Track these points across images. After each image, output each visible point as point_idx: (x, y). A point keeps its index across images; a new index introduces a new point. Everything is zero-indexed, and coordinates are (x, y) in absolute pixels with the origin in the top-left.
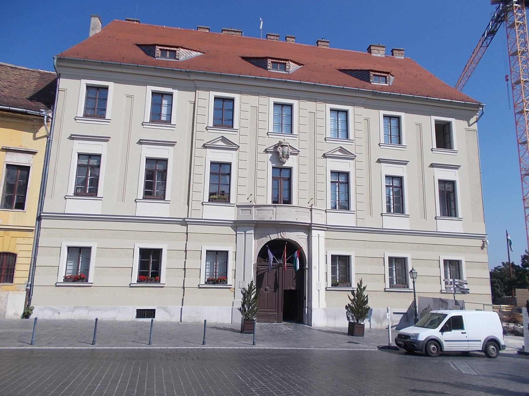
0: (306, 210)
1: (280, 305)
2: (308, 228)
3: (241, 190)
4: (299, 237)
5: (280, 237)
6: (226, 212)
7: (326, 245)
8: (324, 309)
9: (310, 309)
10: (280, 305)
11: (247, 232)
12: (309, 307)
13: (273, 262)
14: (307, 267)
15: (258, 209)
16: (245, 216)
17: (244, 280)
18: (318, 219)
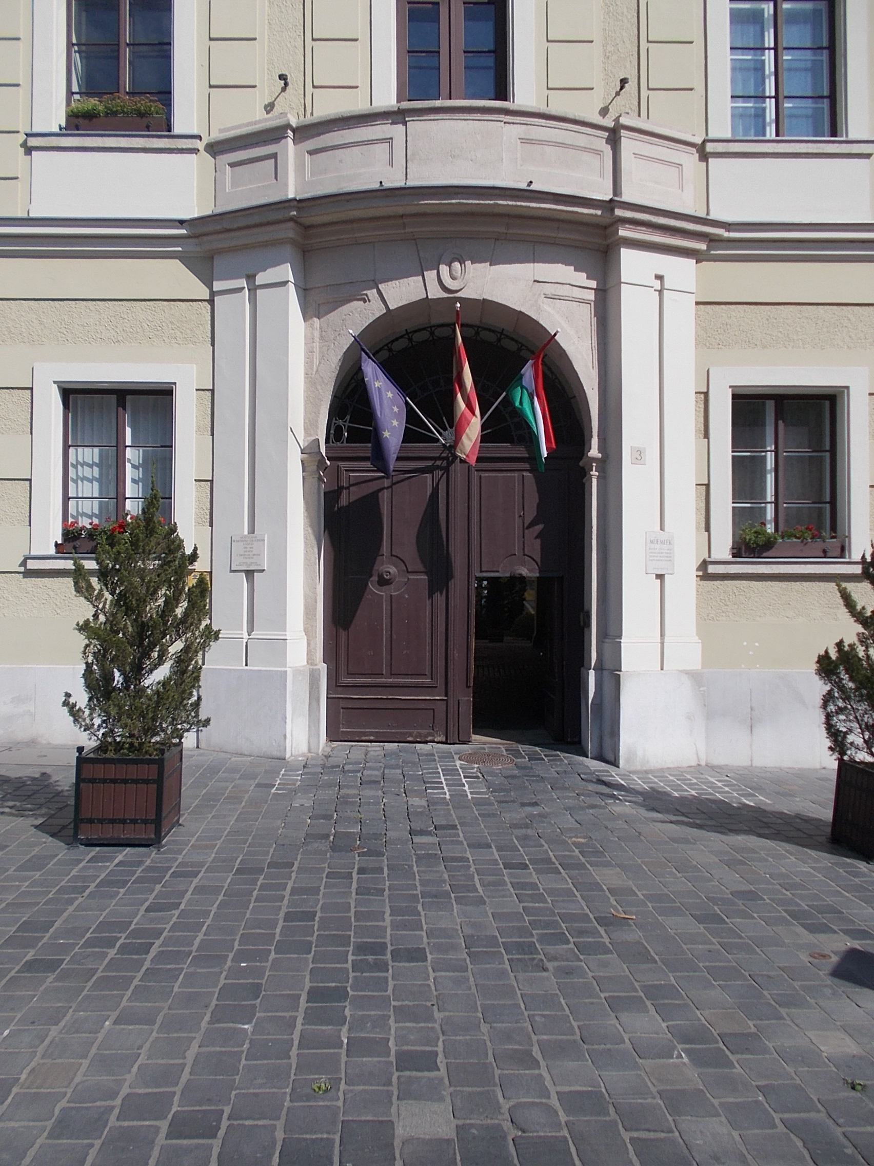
0: (584, 137)
1: (457, 655)
2: (591, 236)
3: (231, 63)
4: (549, 289)
5: (435, 293)
6: (165, 185)
7: (706, 340)
8: (694, 676)
9: (611, 675)
10: (457, 655)
11: (260, 279)
12: (608, 664)
13: (409, 436)
14: (594, 452)
15: (312, 144)
16: (249, 189)
17: (252, 530)
18: (654, 181)
